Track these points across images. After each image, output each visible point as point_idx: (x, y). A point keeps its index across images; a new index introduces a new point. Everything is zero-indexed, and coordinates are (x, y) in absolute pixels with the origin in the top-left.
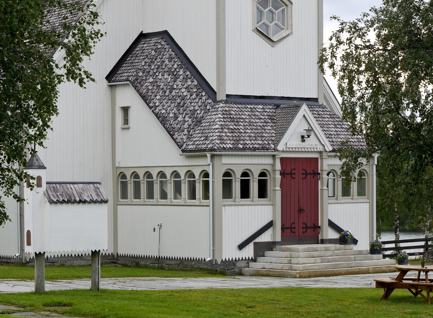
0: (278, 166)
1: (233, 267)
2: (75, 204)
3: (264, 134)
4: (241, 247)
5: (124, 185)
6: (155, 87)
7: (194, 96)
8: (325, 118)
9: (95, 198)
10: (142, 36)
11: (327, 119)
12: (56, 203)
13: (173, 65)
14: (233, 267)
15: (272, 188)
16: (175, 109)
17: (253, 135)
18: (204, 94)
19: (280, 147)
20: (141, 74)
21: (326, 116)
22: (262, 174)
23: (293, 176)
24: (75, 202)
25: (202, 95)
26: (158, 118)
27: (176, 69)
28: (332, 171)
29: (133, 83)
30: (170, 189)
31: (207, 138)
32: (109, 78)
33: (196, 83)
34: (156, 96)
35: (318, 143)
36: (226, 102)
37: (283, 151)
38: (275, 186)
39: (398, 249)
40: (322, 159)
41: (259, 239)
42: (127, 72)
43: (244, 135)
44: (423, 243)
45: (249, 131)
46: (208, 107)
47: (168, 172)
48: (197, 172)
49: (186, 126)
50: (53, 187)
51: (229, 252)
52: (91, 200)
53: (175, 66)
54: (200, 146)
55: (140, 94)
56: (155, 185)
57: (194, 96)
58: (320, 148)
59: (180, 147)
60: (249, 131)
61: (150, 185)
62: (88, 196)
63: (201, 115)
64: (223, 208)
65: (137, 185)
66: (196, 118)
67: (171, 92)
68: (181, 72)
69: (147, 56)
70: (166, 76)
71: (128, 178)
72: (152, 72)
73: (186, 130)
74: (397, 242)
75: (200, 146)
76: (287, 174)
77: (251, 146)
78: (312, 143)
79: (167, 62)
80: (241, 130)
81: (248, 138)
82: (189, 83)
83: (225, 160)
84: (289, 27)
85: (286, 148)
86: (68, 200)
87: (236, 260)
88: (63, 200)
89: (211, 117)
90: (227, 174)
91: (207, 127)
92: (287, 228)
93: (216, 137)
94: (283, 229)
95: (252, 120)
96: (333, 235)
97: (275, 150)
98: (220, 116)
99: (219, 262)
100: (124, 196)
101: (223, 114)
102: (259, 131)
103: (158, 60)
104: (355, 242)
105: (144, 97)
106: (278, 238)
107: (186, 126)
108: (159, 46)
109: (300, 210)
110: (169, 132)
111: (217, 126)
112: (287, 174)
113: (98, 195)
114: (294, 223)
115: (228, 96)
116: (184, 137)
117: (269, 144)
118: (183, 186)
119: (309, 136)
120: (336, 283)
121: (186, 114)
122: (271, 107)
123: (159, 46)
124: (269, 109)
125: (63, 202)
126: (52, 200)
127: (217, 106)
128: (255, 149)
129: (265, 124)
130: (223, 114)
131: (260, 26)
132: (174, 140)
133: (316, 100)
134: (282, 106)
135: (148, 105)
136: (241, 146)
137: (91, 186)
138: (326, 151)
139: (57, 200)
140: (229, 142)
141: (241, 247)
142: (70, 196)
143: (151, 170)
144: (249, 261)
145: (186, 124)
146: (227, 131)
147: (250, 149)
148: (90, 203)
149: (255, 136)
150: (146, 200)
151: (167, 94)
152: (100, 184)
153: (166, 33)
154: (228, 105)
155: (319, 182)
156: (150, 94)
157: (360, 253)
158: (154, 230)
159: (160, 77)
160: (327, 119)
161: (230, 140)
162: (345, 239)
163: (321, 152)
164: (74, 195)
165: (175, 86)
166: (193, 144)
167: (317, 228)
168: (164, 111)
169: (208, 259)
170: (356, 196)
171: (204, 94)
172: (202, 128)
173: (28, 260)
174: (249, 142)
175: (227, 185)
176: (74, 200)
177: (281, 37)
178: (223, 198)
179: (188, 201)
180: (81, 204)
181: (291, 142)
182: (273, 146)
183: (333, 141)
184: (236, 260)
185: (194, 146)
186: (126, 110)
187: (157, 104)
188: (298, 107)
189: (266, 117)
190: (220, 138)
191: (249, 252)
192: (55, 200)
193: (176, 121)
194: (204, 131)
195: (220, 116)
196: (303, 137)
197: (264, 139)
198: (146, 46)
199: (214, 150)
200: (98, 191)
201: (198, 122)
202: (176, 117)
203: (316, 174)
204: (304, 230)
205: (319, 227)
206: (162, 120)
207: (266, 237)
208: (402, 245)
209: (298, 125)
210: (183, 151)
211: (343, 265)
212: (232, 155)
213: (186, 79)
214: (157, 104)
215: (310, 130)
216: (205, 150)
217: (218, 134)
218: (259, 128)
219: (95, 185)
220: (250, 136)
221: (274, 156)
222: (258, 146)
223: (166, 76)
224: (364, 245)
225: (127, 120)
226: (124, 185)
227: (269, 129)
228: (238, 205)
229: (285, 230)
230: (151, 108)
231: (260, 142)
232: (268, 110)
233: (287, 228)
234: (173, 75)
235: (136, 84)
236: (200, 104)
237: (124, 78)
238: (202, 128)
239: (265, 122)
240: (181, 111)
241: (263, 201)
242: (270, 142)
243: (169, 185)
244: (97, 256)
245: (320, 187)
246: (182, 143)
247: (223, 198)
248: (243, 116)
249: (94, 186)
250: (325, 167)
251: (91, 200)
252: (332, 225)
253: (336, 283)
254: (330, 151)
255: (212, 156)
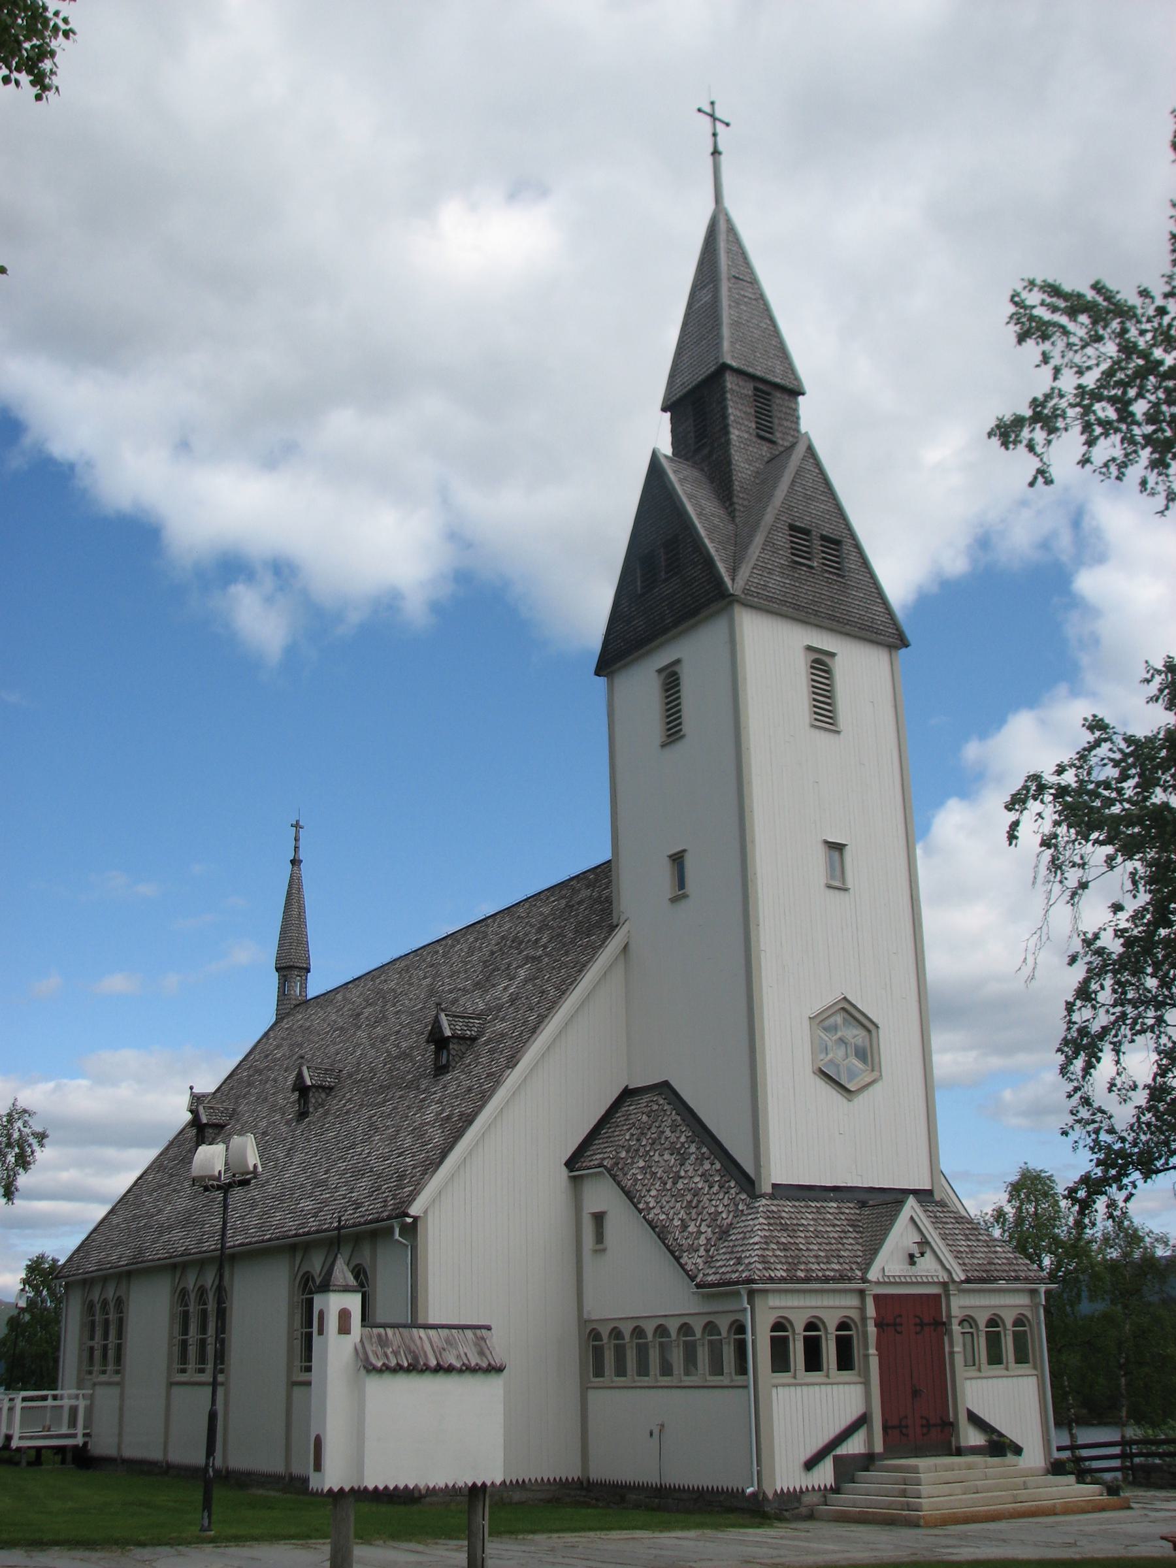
0: (871, 1311)
1: (796, 1505)
2: (427, 1373)
3: (842, 1253)
4: (810, 1464)
5: (598, 1353)
6: (648, 1176)
7: (716, 1188)
8: (946, 1223)
9: (474, 1360)
10: (628, 1094)
11: (950, 1226)
12: (380, 1371)
13: (678, 1138)
14: (796, 1505)
15: (862, 1352)
16: (682, 1212)
17: (822, 1254)
18: (732, 1184)
19: (873, 1275)
20: (623, 1154)
21: (948, 1220)
22: (843, 1326)
23: (899, 1328)
24: (425, 1369)
25: (730, 1187)
26: (653, 1228)
27: (683, 1144)
28: (968, 1320)
29: (609, 1170)
30: (677, 1357)
31: (739, 1261)
32: (570, 1164)
33: (718, 1166)
34: (649, 1191)
35: (939, 1267)
36: (772, 1197)
37: (878, 1283)
38: (866, 1347)
39: (1079, 1460)
40: (948, 1296)
41: (842, 1450)
42: (602, 1154)
43: (806, 1254)
44: (1117, 1450)
45: (816, 1248)
46: (740, 1207)
47: (673, 1326)
48: (724, 1324)
49: (702, 1241)
50: (379, 1335)
51: (786, 1474)
52: (464, 1364)
53: (683, 1139)
54: (728, 1276)
55: (622, 1189)
56: (651, 1352)
57: (716, 1188)
58: (943, 1276)
59: (692, 1278)
60: (816, 1248)
61: (643, 1351)
62: (458, 1357)
63: (729, 1221)
64: (774, 1390)
65: (620, 1352)
66: (720, 1227)
67: (675, 1183)
68: (693, 1149)
69: (634, 1124)
70: (666, 1157)
71: (605, 1340)
72: (642, 1150)
73: (702, 1249)
74: (1073, 1448)
75: (728, 1276)
76: (888, 1325)
77: (820, 1274)
78: (927, 1266)
79: (668, 1133)
80: (801, 1246)
81: (813, 1260)
82: (707, 1166)
83: (774, 1301)
84: (876, 1068)
85: (884, 1275)
86: (409, 1365)
87: (801, 1491)
88: (398, 1364)
89: (747, 1223)
90: (778, 1326)
91: (740, 1242)
92: (894, 1427)
93: (756, 1258)
94: (885, 1428)
95: (820, 1228)
96: (973, 1437)
97: (864, 1280)
98: (762, 1220)
99: (770, 1495)
100: (599, 1372)
101: (769, 1217)
102: (834, 1247)
103: (653, 1130)
104: (1018, 1451)
105: (628, 1194)
106: (879, 1448)
107: (702, 1241)
108: (655, 1107)
109: (915, 1393)
110: (672, 1253)
111: (756, 1239)
112: (888, 1325)
113: (481, 1353)
114: (906, 1417)
115: (774, 1186)
116: (699, 1260)
117: (852, 1269)
118: (700, 1350)
119: (922, 1254)
120: (1004, 1541)
121: (702, 1220)
122: (851, 1205)
123: (655, 1107)
124: (849, 1209)
125: (398, 1369)
126: (371, 1364)
127: (757, 1204)
128: (827, 1280)
129: (842, 1235)
130: (769, 1217)
131: (825, 1065)
132: (682, 1266)
133: (930, 1192)
134: (871, 1203)
135: (635, 1206)
136: (801, 1274)
137: (469, 1333)
138: (954, 1281)
139: (384, 1364)
140: (779, 1267)
141: (810, 1464)
142: (416, 1358)
143: (641, 1323)
144: (825, 1492)
145: (703, 1237)
146: (775, 1247)
147: (817, 1279)
148: (460, 1371)
149: (826, 1257)
150: (637, 1378)
151: (668, 1187)
152: (489, 1328)
153: (666, 1084)
154: (775, 1202)
155: (946, 1339)
156: (638, 1187)
157: (1031, 1473)
158: (651, 1434)
159: (656, 1158)
160: (950, 1226)
161: (781, 1263)
162: (1000, 1446)
163: (945, 1285)
164: (425, 1353)
165: (682, 1173)
166: (715, 1273)
167: (948, 1426)
168: (663, 1217)
169: (749, 1490)
170: (1012, 1364)
171: (732, 1184)
172: (731, 1244)
173: (423, 1492)
174: (816, 1266)
175: (780, 1349)
176: (425, 1364)
177: (863, 1083)
178: (773, 1371)
179: (709, 1378)
180: (440, 1373)
181: (889, 1263)
182: (859, 1273)
183: (964, 1264)
184: (801, 1491)
185: (718, 1277)
186: (599, 1218)
187: (651, 1205)
188: (901, 1203)
189: (845, 1223)
190: (764, 1260)
191: (825, 1474)
192: (379, 1364)
193: (686, 1234)
194: (736, 1249)
195: (762, 1220)
196: (911, 1256)
197: (841, 1260)
198: (636, 1111)
199: (753, 1281)
200: (483, 1343)
201: (724, 1233)
202: (684, 1227)
203: (940, 1326)
204: (925, 1430)
205: (951, 1424)
206: (660, 1232)
207: (855, 1446)
208: (1085, 1453)
209: (901, 1236)
210: (698, 1286)
211: (1000, 1500)
212: (786, 1291)
213: (700, 1160)
214: (651, 1205)
215: (924, 1243)
216: (737, 1283)
217: (759, 1252)
218: (833, 1241)
219: (478, 1332)
220: (816, 1257)
221: (862, 1293)
222: (832, 1274)
223: (666, 1157)
224: (1034, 1457)
225: (602, 1233)
226: (598, 1353)
227: (851, 1244)
228: (801, 1385)
229: (890, 1431)
230: (640, 1211)
231: (837, 1267)
232: (847, 1211)
233: (894, 1427)
234: (679, 1153)
235: (614, 1174)
236: (726, 1202)
237: (596, 1162)
238: (731, 1244)
239: (843, 1231)
240: (694, 1216)
241: (846, 1375)
242: (854, 1267)
243: (675, 1350)
244: (481, 1497)
245: (947, 1349)
246: (695, 1271)
247: (773, 1371)
248: (803, 1222)
249: (475, 1334)
250: (955, 1311)
251: (464, 1364)
252: (974, 1419)
253: (1004, 1541)
254: (962, 1282)
255: (751, 1294)
